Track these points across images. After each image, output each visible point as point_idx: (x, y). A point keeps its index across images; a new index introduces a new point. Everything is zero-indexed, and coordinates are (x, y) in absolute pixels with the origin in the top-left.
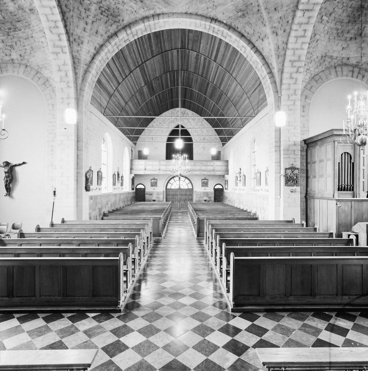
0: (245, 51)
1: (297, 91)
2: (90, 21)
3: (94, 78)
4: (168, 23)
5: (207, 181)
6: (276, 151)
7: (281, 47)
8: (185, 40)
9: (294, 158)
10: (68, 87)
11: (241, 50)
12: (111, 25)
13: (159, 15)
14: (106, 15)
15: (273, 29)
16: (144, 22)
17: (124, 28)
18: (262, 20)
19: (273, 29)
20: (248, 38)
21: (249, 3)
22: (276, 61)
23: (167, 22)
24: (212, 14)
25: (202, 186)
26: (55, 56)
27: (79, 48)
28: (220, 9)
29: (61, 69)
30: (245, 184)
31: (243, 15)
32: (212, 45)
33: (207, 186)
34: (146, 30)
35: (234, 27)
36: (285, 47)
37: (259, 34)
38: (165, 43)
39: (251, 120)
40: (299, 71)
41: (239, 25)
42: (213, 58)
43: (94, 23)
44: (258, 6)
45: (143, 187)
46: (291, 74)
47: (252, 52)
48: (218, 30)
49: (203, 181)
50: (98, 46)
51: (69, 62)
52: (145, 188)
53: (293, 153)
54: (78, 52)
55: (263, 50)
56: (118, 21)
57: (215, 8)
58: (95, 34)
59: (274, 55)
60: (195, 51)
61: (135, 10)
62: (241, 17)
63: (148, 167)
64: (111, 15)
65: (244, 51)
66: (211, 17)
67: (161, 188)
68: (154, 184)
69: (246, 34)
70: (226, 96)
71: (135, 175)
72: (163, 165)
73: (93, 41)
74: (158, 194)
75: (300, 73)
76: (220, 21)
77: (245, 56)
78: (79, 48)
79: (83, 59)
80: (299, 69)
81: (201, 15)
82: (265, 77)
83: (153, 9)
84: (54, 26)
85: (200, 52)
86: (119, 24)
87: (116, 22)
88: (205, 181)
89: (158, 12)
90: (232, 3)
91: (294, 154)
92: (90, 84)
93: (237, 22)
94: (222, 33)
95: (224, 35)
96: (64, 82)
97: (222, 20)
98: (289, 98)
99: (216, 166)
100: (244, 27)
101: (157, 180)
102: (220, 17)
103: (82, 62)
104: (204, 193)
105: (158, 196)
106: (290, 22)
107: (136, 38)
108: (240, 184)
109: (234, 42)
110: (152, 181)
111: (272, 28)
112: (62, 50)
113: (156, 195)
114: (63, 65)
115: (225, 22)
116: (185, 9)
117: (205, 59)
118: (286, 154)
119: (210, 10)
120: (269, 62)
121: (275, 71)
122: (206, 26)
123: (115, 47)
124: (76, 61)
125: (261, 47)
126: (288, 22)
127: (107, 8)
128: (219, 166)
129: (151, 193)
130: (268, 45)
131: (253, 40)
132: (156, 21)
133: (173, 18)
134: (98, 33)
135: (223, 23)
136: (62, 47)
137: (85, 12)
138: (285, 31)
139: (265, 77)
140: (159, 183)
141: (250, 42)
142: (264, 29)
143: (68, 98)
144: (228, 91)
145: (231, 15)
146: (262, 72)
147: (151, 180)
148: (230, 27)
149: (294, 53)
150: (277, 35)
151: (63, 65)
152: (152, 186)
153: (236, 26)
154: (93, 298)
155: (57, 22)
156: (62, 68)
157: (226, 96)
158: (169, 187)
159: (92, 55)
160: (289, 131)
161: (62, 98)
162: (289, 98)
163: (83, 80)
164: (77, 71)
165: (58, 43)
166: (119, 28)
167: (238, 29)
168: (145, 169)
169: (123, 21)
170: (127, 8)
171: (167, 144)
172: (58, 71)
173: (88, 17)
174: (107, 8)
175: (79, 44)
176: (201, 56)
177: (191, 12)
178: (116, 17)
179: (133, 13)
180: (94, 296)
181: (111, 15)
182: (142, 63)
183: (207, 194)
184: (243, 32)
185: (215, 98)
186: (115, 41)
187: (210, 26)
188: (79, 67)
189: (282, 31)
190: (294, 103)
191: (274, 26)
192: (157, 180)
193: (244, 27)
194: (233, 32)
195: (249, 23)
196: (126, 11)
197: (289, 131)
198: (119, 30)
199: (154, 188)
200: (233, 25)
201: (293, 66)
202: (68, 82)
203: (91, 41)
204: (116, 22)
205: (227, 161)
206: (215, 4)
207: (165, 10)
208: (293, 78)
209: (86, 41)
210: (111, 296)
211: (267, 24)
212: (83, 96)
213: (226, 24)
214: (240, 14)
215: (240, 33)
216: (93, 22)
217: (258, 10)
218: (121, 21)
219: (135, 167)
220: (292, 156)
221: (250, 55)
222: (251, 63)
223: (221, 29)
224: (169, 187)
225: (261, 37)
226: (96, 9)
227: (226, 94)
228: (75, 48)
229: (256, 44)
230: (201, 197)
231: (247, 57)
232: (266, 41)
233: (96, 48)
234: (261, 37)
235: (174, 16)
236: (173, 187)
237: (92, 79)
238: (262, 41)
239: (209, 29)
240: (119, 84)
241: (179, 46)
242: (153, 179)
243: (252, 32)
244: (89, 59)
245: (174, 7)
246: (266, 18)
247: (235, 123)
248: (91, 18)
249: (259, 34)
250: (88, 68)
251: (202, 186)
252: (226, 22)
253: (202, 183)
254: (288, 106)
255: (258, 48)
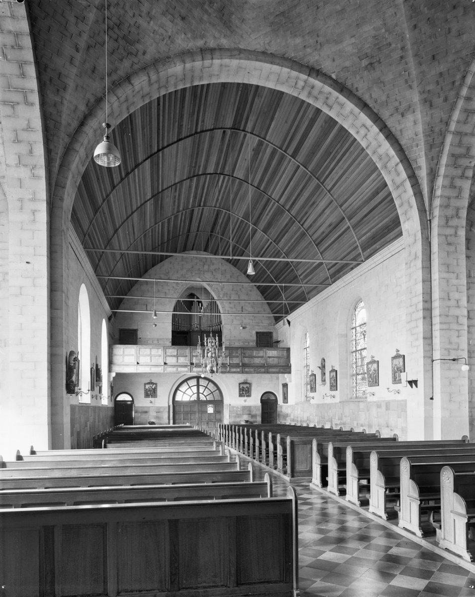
0: (366, 135)
1: (461, 211)
2: (82, 44)
3: (80, 166)
4: (227, 68)
5: (248, 385)
6: (424, 318)
7: (437, 130)
8: (244, 111)
9: (457, 330)
10: (34, 177)
11: (358, 132)
12: (121, 60)
13: (212, 50)
14: (115, 36)
15: (425, 96)
16: (184, 62)
17: (144, 69)
18: (407, 77)
19: (425, 96)
20: (375, 110)
21: (385, 43)
22: (426, 154)
23: (226, 66)
24: (313, 58)
25: (240, 395)
26: (8, 110)
27: (58, 99)
28: (328, 50)
29: (20, 138)
30: (334, 387)
31: (371, 64)
32: (296, 123)
33: (249, 396)
34: (184, 79)
35: (350, 87)
36: (443, 129)
37: (397, 104)
38: (207, 113)
39: (352, 269)
40: (466, 175)
41: (361, 85)
42: (291, 150)
43: (91, 51)
44: (403, 48)
45: (129, 398)
46: (453, 179)
47: (381, 137)
48: (321, 92)
49: (241, 387)
50: (92, 100)
51: (37, 123)
52: (133, 401)
53: (456, 321)
54: (55, 105)
55: (402, 134)
56: (134, 53)
57: (319, 47)
58: (89, 72)
59: (423, 144)
60: (258, 136)
61: (170, 34)
62: (366, 68)
63: (142, 360)
64: (124, 38)
65: (363, 135)
66: (310, 64)
67: (163, 401)
68: (151, 393)
69: (369, 102)
70: (302, 225)
71: (117, 374)
72: (171, 356)
73: (84, 86)
74: (158, 411)
75: (467, 178)
76: (325, 75)
77: (364, 144)
78: (58, 99)
79: (64, 122)
80: (466, 171)
81: (290, 59)
82: (402, 183)
83: (202, 37)
84: (13, 44)
85: (267, 139)
86: (136, 60)
87: (131, 54)
88: (245, 386)
89: (212, 44)
90: (353, 40)
91: (458, 323)
92: (73, 177)
93: (358, 77)
94: (327, 98)
95: (330, 102)
96: (25, 166)
97: (329, 73)
98: (447, 222)
99: (269, 357)
100: (369, 89)
101: (156, 384)
102: (327, 66)
103: (62, 128)
104: (244, 408)
105: (159, 414)
106: (457, 84)
107: (163, 92)
108: (323, 389)
109: (345, 118)
110: (147, 386)
111: (424, 92)
112: (25, 97)
113: (155, 414)
114: (23, 130)
115: (334, 76)
116: (262, 44)
117: (274, 152)
118: (445, 323)
119: (309, 50)
120: (411, 156)
121: (423, 174)
122: (299, 81)
123: (124, 106)
124: (51, 124)
125: (399, 128)
126: (453, 83)
127: (118, 22)
128: (274, 357)
129: (145, 410)
130: (413, 124)
131: (385, 114)
132: (207, 62)
133: (240, 59)
134: (96, 72)
135: (330, 78)
136: (24, 93)
137: (76, 24)
138: (446, 100)
139: (402, 183)
140: (160, 391)
141: (377, 119)
142: (408, 93)
143: (34, 200)
144: (307, 215)
145: (347, 64)
146: (395, 177)
147: (145, 384)
148: (341, 87)
149: (460, 141)
150: (431, 106)
151: (23, 130)
152: (147, 395)
153: (356, 86)
154: (237, 588)
155: (20, 36)
156: (23, 136)
157: (302, 225)
158: (179, 398)
159: (81, 117)
160: (448, 281)
161: (21, 200)
162: (447, 222)
163: (61, 166)
164: (52, 147)
165: (17, 82)
166: (136, 67)
167: (357, 91)
168: (138, 363)
169: (144, 53)
170: (156, 28)
171: (174, 316)
172: (14, 142)
173: (80, 35)
174: (118, 22)
175: (58, 90)
176: (267, 145)
177: (272, 51)
178: (131, 43)
179: (165, 41)
180: (238, 584)
181: (124, 38)
182: (159, 151)
183: (248, 409)
184: (366, 98)
185: (274, 232)
186: (125, 91)
187: (305, 82)
188: (55, 138)
189: (442, 99)
190: (456, 233)
191: (428, 88)
192: (156, 384)
193: (369, 89)
194: (348, 98)
195: (379, 82)
196: (152, 34)
197: (448, 281)
198: (136, 73)
199: (150, 399)
200: (349, 84)
201: (455, 166)
202: (34, 167)
203: (82, 87)
204: (131, 54)
205: (288, 350)
206: (321, 39)
207: (224, 42)
208: (455, 187)
209: (71, 84)
210: (275, 582)
211: (415, 84)
212: (62, 199)
213: (335, 81)
214: (365, 63)
215: (360, 99)
216: (89, 47)
217: (402, 57)
218: (140, 53)
219: (117, 359)
220: (454, 326)
221: (374, 143)
222: (375, 159)
223: (327, 89)
224: (179, 398)
225: (401, 110)
226: (97, 21)
227: (301, 223)
228: (51, 97)
229: (389, 123)
230: (238, 416)
231: (367, 148)
232: (410, 117)
233: (89, 104)
234: (401, 110)
235: (242, 55)
236: (186, 398)
237: (77, 167)
238: (400, 116)
239: (303, 88)
240: (114, 187)
241: (229, 123)
242: (148, 383)
243: (384, 98)
244: (75, 124)
245: (242, 37)
246: (414, 72)
247: (312, 278)
248: (85, 37)
249: (397, 104)
250: (71, 143)
251: (240, 395)
252: (337, 76)
253: (240, 390)
254: (446, 236)
255: (393, 130)
